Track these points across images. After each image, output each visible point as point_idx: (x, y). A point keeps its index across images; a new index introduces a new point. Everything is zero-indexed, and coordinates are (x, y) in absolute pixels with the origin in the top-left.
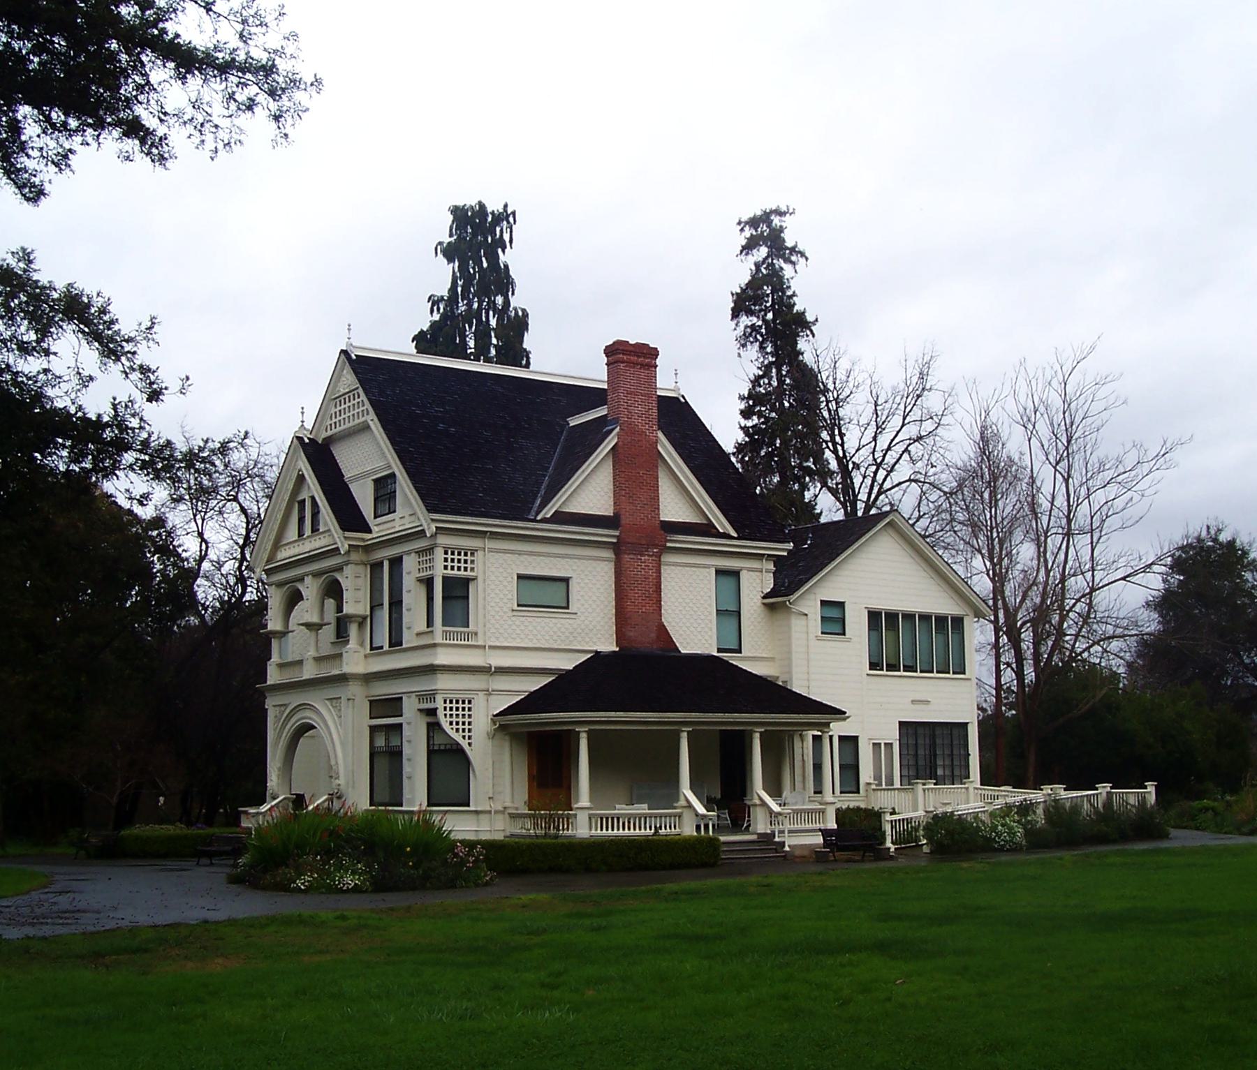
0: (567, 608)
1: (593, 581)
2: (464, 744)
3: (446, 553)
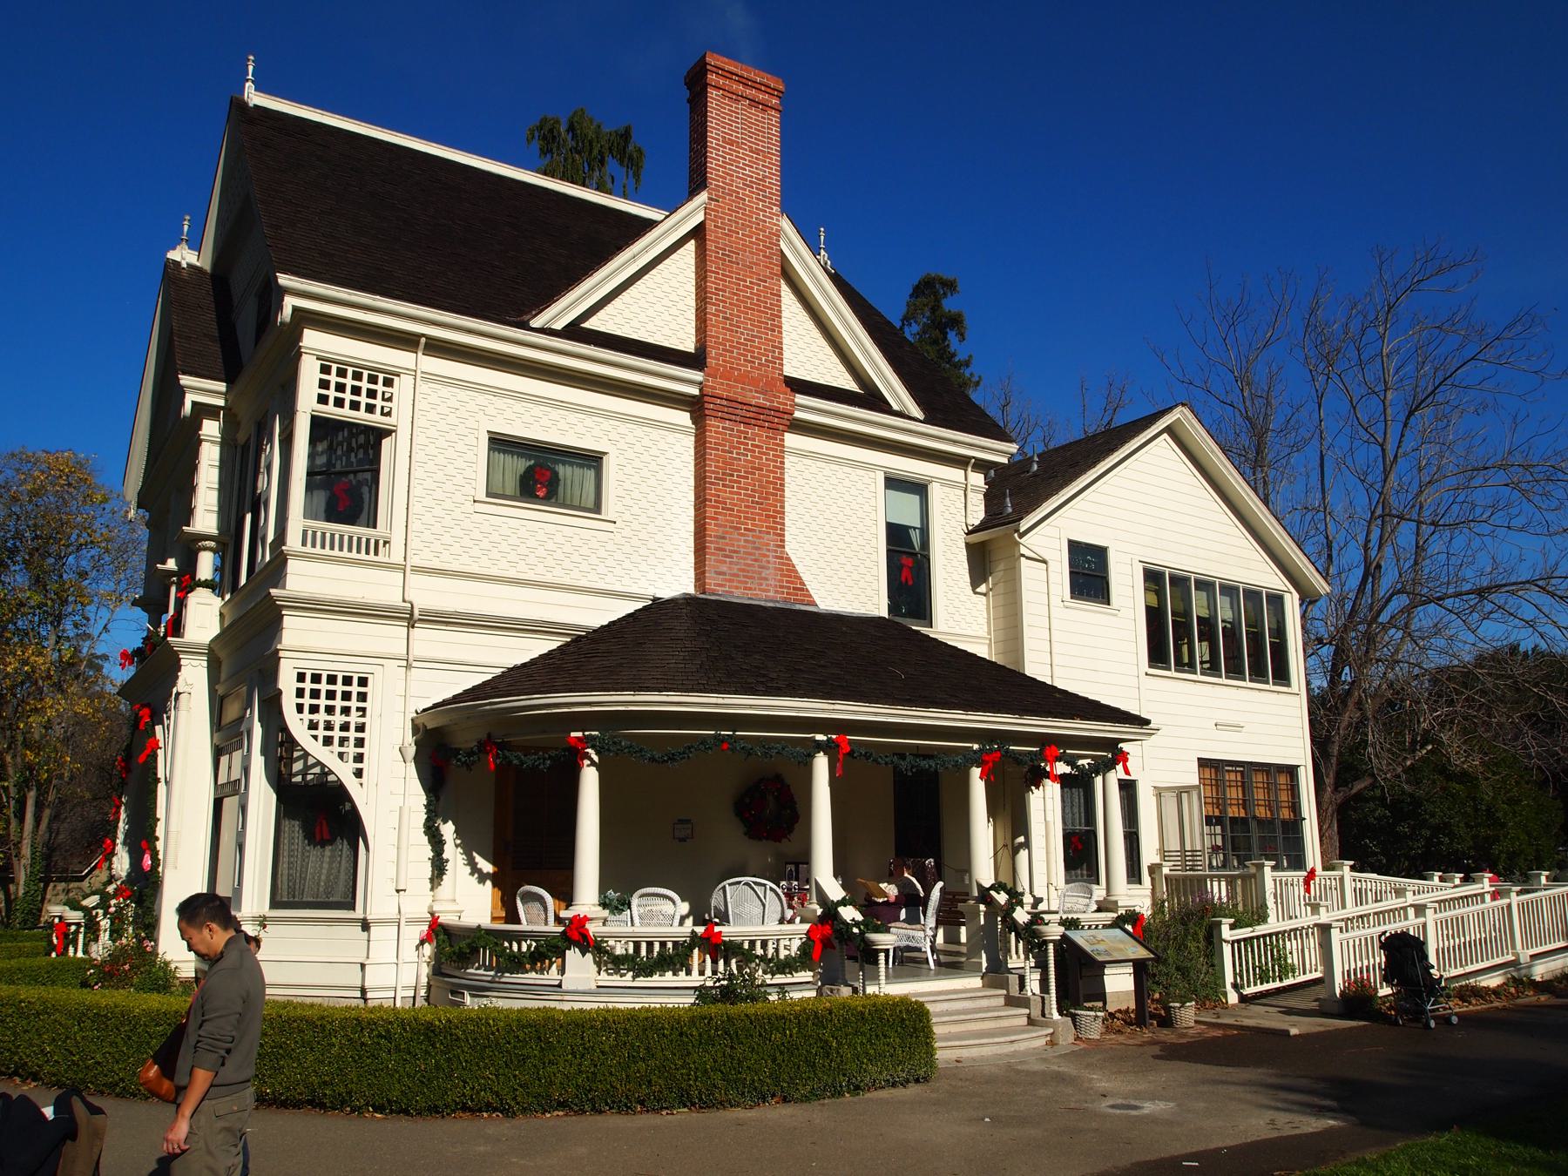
0: (599, 512)
1: (649, 460)
2: (343, 772)
3: (325, 369)
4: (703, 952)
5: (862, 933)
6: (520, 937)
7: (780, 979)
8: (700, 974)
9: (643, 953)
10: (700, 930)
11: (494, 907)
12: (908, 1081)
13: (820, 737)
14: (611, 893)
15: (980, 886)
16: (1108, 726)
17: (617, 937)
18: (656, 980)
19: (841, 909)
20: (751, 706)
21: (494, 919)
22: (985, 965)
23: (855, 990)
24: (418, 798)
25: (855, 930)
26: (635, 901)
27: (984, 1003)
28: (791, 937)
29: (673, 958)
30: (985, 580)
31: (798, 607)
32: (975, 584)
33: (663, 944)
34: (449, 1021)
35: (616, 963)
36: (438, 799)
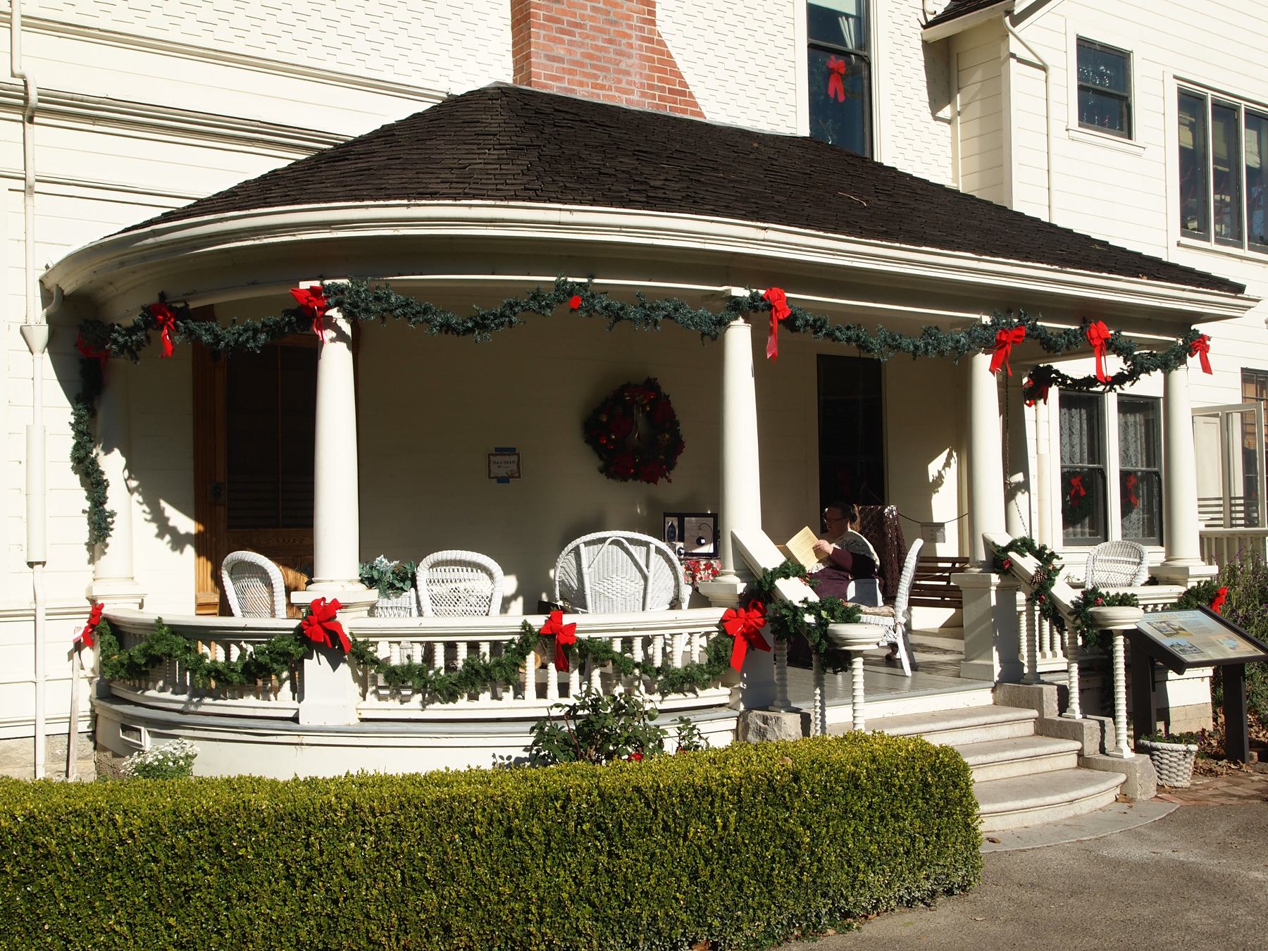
4: (541, 652)
5: (822, 624)
6: (225, 637)
7: (675, 700)
8: (542, 696)
9: (440, 661)
10: (538, 621)
11: (200, 588)
12: (933, 894)
13: (739, 292)
14: (382, 562)
15: (989, 544)
16: (1187, 292)
17: (394, 637)
18: (463, 707)
19: (781, 583)
20: (621, 228)
21: (200, 606)
22: (997, 669)
23: (806, 720)
24: (56, 412)
25: (809, 619)
26: (423, 573)
27: (1004, 732)
28: (688, 634)
29: (491, 670)
30: (949, 99)
31: (678, 115)
32: (937, 102)
33: (473, 647)
34: (30, 817)
35: (397, 679)
36: (92, 412)
